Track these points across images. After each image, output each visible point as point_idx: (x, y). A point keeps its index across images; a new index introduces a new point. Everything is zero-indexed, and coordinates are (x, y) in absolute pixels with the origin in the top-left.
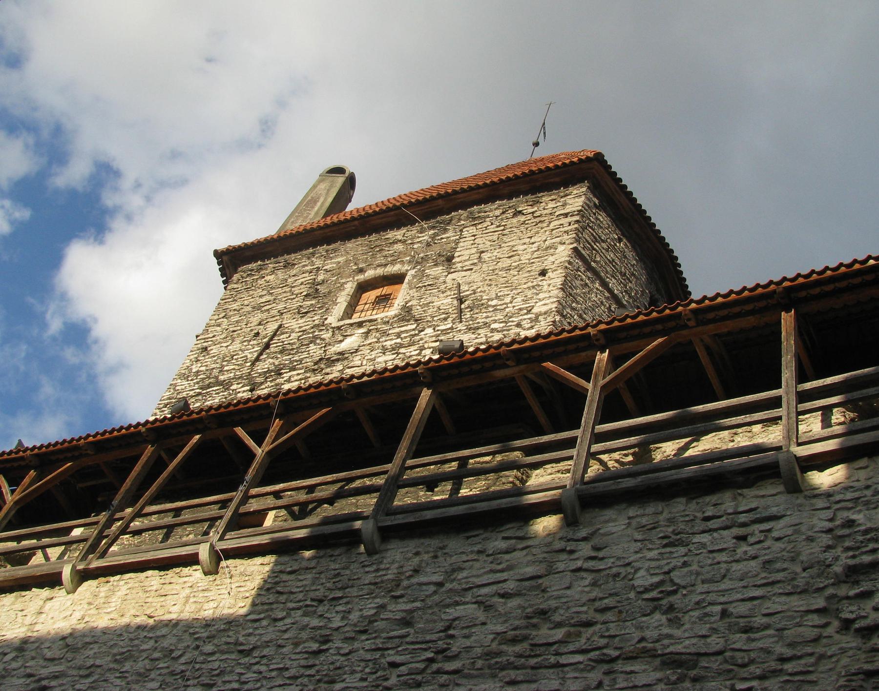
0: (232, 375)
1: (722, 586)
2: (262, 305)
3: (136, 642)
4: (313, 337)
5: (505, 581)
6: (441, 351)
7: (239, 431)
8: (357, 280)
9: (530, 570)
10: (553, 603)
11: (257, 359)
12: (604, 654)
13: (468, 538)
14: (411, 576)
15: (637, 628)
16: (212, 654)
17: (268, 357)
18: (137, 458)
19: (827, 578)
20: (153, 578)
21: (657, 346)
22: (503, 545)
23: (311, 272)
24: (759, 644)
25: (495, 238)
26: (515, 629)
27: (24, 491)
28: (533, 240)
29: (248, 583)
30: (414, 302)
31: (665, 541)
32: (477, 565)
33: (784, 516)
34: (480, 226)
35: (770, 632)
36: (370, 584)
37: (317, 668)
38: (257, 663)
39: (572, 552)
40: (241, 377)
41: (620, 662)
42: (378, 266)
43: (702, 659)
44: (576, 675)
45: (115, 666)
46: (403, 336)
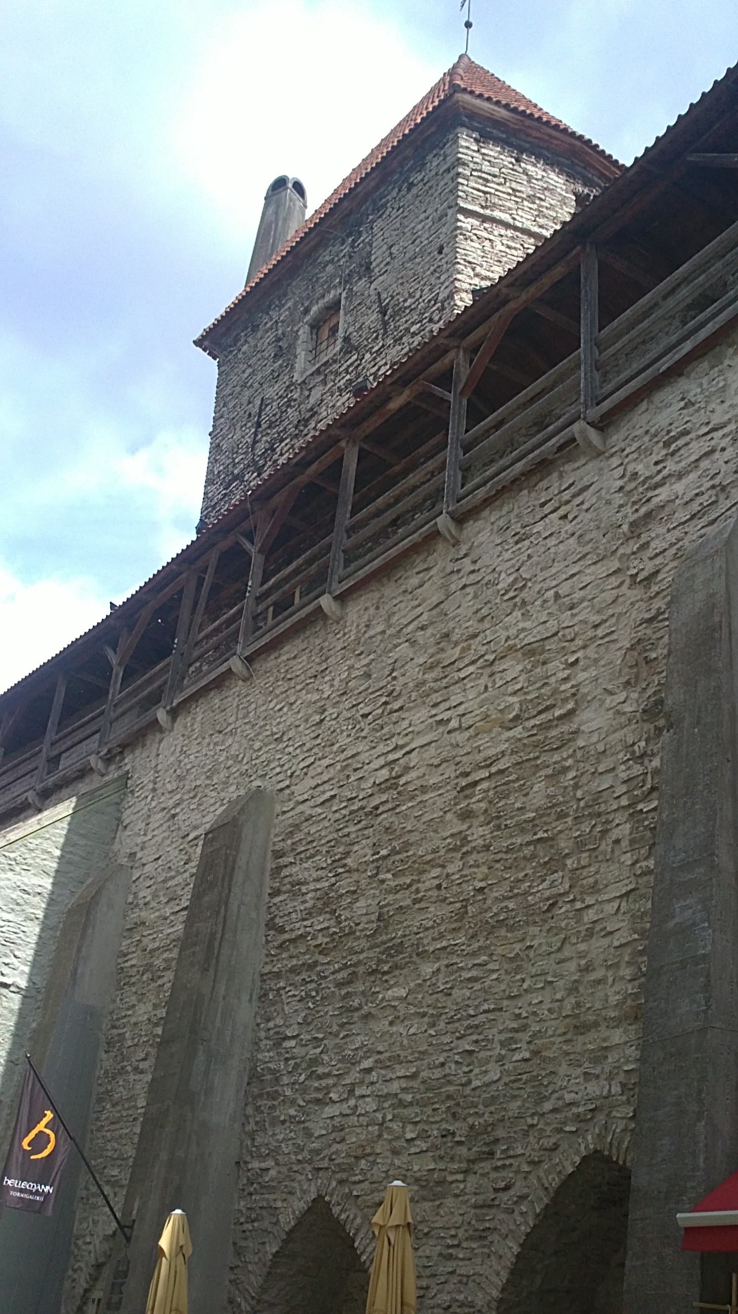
0: (242, 466)
1: (554, 570)
3: (216, 757)
4: (288, 401)
5: (422, 614)
9: (435, 600)
10: (451, 625)
11: (255, 442)
12: (486, 661)
13: (396, 581)
14: (365, 632)
15: (503, 629)
16: (260, 749)
17: (262, 436)
19: (619, 539)
22: (415, 581)
24: (579, 618)
25: (398, 225)
26: (431, 657)
28: (427, 214)
29: (271, 679)
30: (351, 329)
31: (517, 538)
32: (402, 605)
33: (593, 483)
34: (384, 216)
35: (585, 604)
36: (342, 649)
37: (321, 737)
38: (287, 746)
39: (459, 571)
40: (249, 466)
41: (497, 662)
42: (318, 299)
43: (546, 642)
44: (472, 684)
45: (208, 782)
46: (350, 369)
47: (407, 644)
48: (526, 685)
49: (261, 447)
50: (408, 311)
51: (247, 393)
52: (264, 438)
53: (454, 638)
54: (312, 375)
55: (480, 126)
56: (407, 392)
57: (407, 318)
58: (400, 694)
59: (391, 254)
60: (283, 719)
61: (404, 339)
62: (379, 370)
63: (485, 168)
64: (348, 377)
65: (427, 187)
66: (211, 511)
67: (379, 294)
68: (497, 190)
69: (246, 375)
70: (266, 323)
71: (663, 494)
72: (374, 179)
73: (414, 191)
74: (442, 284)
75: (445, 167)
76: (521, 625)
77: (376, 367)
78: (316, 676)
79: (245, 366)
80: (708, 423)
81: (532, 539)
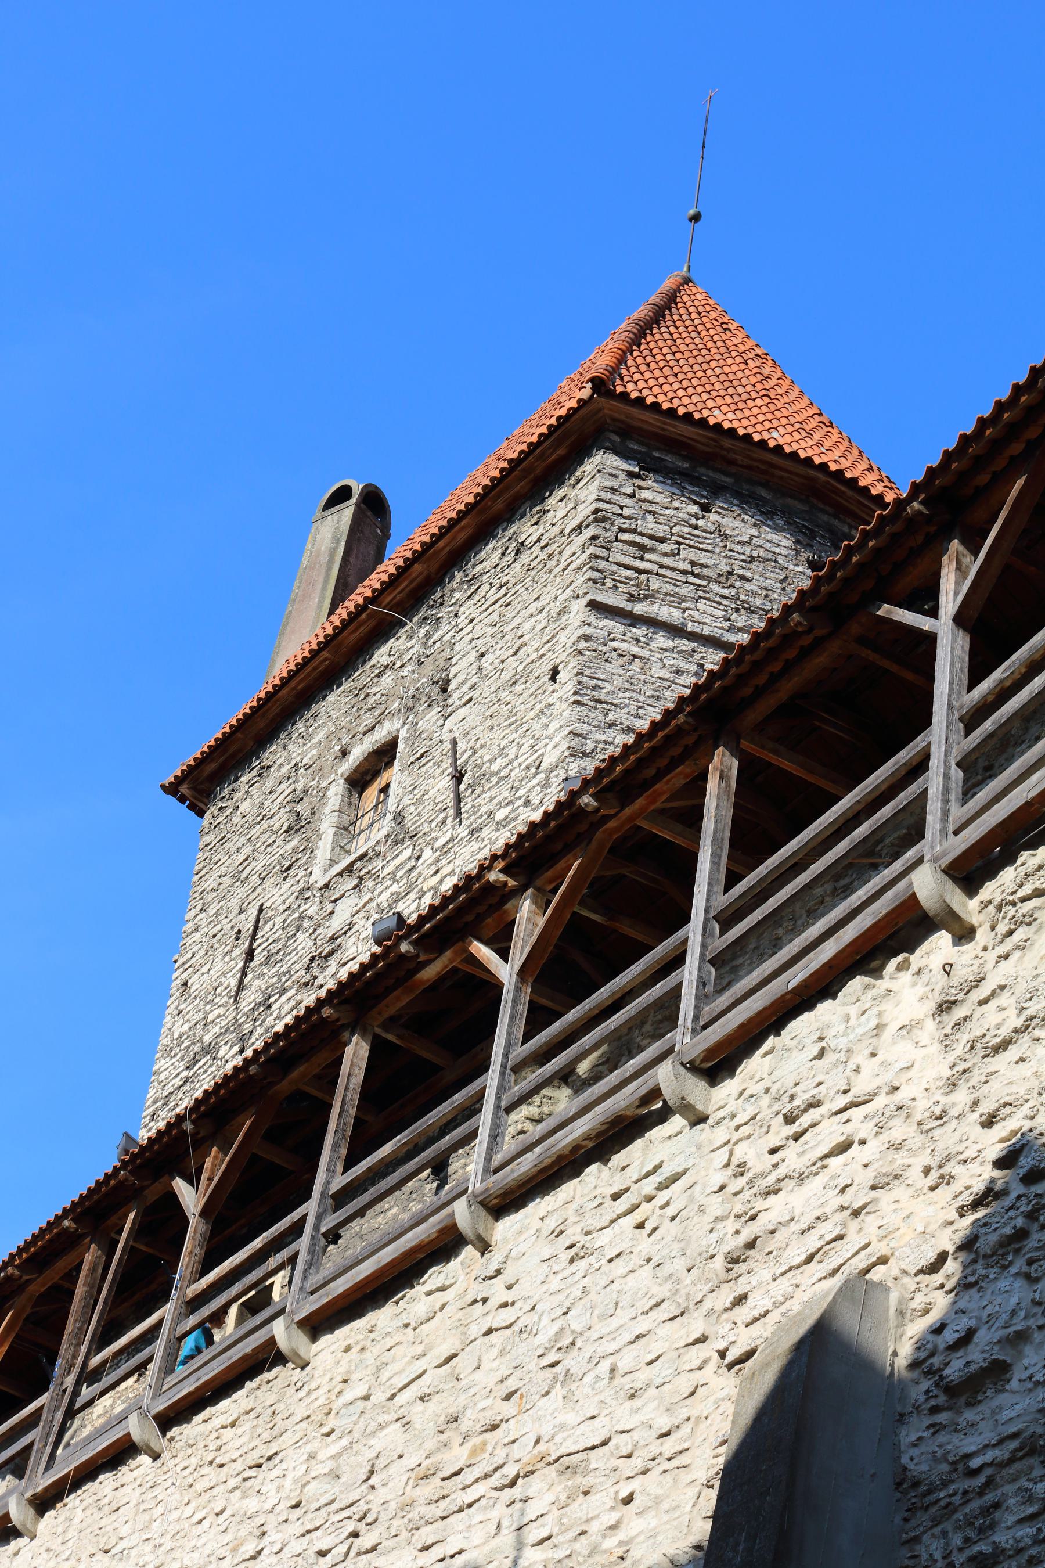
2: (241, 868)
6: (378, 942)
7: (885, 610)
8: (342, 775)
11: (240, 987)
13: (397, 1303)
18: (78, 1267)
20: (106, 1480)
21: (133, 1223)
23: (289, 778)
27: (207, 1190)
41: (520, 1481)
44: (480, 1518)
47: (399, 1424)
48: (555, 1531)
49: (250, 997)
50: (494, 780)
51: (241, 892)
52: (257, 983)
53: (465, 1424)
54: (340, 874)
55: (643, 449)
56: (448, 954)
57: (492, 793)
58: (375, 1521)
59: (480, 668)
60: (202, 1541)
61: (485, 833)
62: (441, 882)
63: (641, 525)
64: (395, 888)
65: (543, 556)
66: (162, 1108)
67: (454, 742)
68: (661, 566)
69: (241, 857)
70: (281, 766)
71: (775, 1209)
72: (463, 528)
73: (526, 558)
74: (550, 738)
75: (575, 523)
76: (561, 1418)
77: (438, 877)
78: (259, 1466)
79: (242, 840)
80: (846, 1092)
81: (592, 1259)
